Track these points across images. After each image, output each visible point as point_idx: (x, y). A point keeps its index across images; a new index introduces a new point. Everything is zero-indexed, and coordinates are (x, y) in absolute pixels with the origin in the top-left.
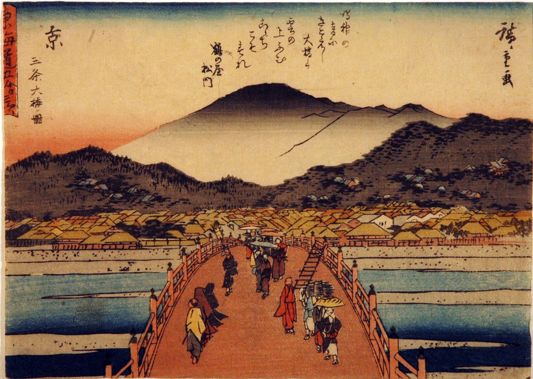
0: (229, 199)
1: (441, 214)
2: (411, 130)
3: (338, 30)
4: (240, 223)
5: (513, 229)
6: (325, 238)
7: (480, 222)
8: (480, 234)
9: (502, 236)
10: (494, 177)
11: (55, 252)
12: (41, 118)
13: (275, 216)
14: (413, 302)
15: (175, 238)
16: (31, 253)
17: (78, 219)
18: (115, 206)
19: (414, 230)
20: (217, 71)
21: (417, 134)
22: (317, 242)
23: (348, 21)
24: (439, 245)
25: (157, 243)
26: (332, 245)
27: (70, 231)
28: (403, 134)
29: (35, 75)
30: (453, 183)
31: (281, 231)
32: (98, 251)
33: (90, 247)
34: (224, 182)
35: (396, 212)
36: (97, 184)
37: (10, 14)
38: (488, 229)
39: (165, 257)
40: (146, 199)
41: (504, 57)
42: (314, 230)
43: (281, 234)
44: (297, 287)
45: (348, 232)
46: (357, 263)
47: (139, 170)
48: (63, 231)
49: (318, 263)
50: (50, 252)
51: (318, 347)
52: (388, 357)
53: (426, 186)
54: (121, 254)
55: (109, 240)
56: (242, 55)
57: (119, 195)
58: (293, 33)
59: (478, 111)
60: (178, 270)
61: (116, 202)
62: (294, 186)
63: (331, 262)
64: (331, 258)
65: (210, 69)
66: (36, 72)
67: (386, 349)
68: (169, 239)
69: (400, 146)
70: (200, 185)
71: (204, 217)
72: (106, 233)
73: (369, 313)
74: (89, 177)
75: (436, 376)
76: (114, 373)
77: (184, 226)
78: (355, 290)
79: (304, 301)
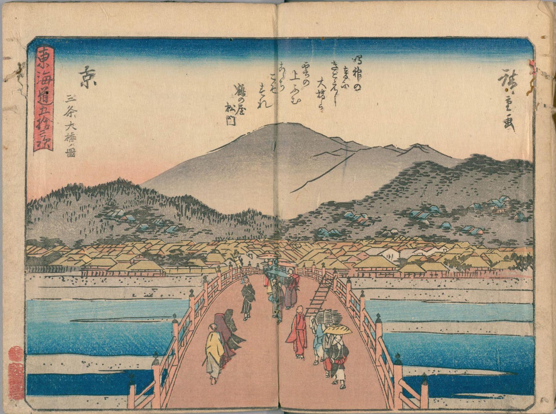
0: (248, 230)
1: (445, 248)
2: (418, 168)
3: (350, 74)
4: (258, 253)
5: (513, 263)
6: (335, 269)
7: (481, 256)
8: (482, 267)
9: (503, 270)
10: (496, 214)
11: (85, 278)
12: (74, 151)
13: (288, 247)
14: (417, 330)
15: (197, 266)
16: (62, 278)
17: (106, 247)
18: (142, 236)
19: (419, 263)
20: (240, 110)
21: (424, 173)
22: (327, 273)
23: (359, 66)
24: (442, 278)
25: (180, 271)
26: (341, 276)
27: (98, 258)
28: (410, 172)
29: (70, 112)
30: (458, 219)
31: (294, 262)
32: (124, 278)
33: (116, 274)
34: (245, 214)
35: (403, 246)
36: (125, 214)
37: (49, 54)
38: (490, 264)
39: (188, 284)
40: (170, 230)
41: (506, 102)
42: (325, 261)
43: (293, 265)
44: (308, 315)
45: (356, 264)
46: (365, 293)
47: (164, 202)
48: (92, 258)
49: (327, 292)
50: (79, 278)
51: (327, 372)
52: (393, 383)
53: (432, 222)
54: (145, 281)
55: (135, 267)
56: (264, 96)
57: (145, 225)
58: (307, 76)
59: (481, 153)
60: (199, 298)
61: (142, 232)
62: (306, 220)
63: (340, 292)
64: (340, 288)
65: (233, 108)
66: (70, 109)
67: (391, 376)
68: (191, 268)
69: (407, 184)
70: (221, 217)
71: (226, 246)
72: (132, 261)
73: (375, 340)
74: (117, 208)
75: (438, 401)
76: (138, 393)
77: (205, 255)
78: (362, 319)
79: (314, 328)
